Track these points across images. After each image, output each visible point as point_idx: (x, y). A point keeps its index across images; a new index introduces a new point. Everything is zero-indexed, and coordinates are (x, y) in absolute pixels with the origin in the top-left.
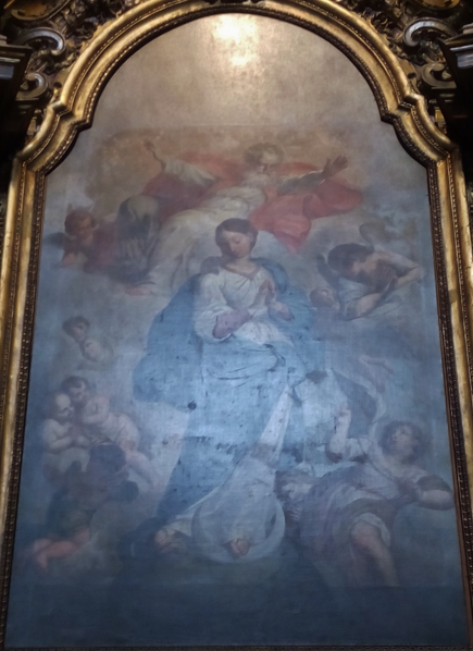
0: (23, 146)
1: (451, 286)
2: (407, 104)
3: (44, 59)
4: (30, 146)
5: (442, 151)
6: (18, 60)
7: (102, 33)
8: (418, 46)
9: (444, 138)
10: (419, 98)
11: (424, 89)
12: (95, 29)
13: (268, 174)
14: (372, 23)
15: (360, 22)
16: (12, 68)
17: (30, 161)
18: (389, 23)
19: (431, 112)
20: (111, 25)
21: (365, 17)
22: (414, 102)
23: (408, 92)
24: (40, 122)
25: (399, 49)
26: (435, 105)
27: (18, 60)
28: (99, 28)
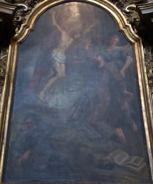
0: (15, 35)
1: (12, 84)
2: (126, 27)
3: (21, 12)
4: (16, 35)
5: (137, 40)
6: (14, 9)
7: (38, 5)
8: (129, 12)
9: (136, 36)
10: (130, 26)
11: (133, 24)
12: (36, 4)
13: (123, 4)
14: (116, 5)
15: (112, 4)
16: (12, 11)
17: (16, 39)
18: (121, 6)
19: (134, 30)
20: (41, 3)
21: (114, 4)
22: (128, 26)
23: (127, 24)
24: (19, 29)
25: (123, 13)
26: (134, 28)
27: (14, 9)
28: (37, 4)
